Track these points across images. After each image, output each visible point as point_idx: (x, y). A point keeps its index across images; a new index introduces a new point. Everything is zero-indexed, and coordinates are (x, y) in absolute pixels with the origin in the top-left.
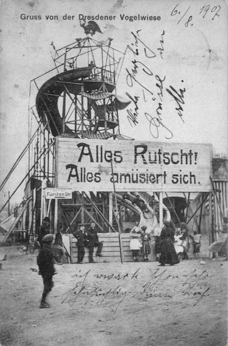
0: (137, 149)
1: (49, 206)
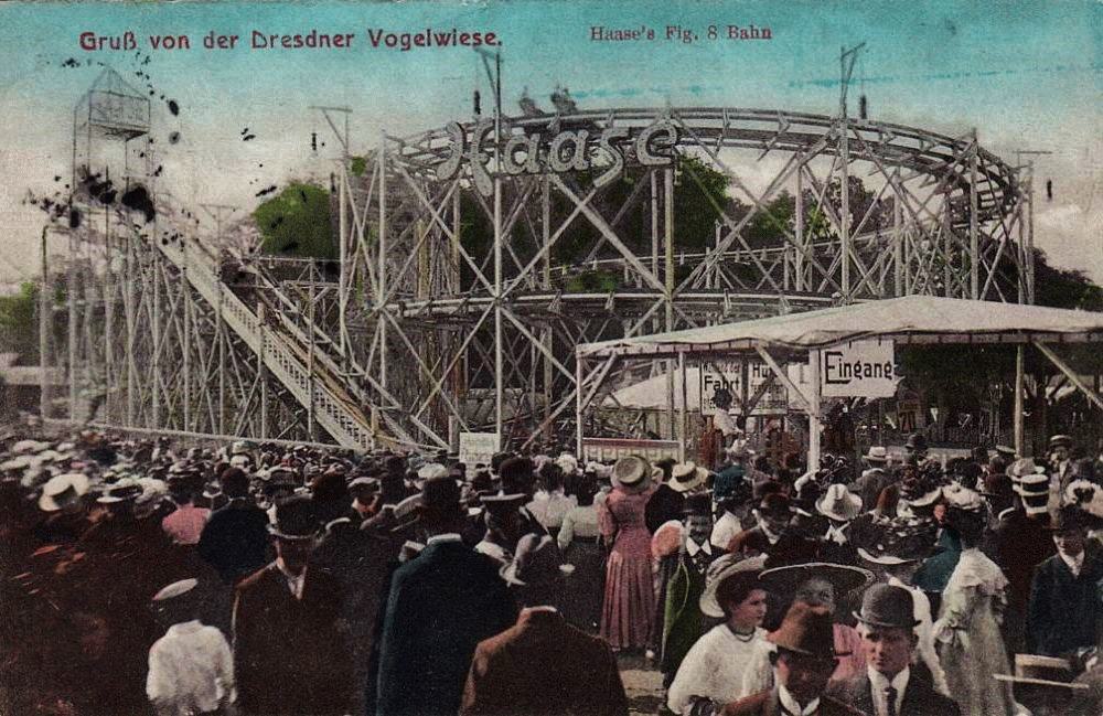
0: (829, 357)
1: (343, 220)
